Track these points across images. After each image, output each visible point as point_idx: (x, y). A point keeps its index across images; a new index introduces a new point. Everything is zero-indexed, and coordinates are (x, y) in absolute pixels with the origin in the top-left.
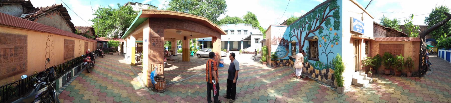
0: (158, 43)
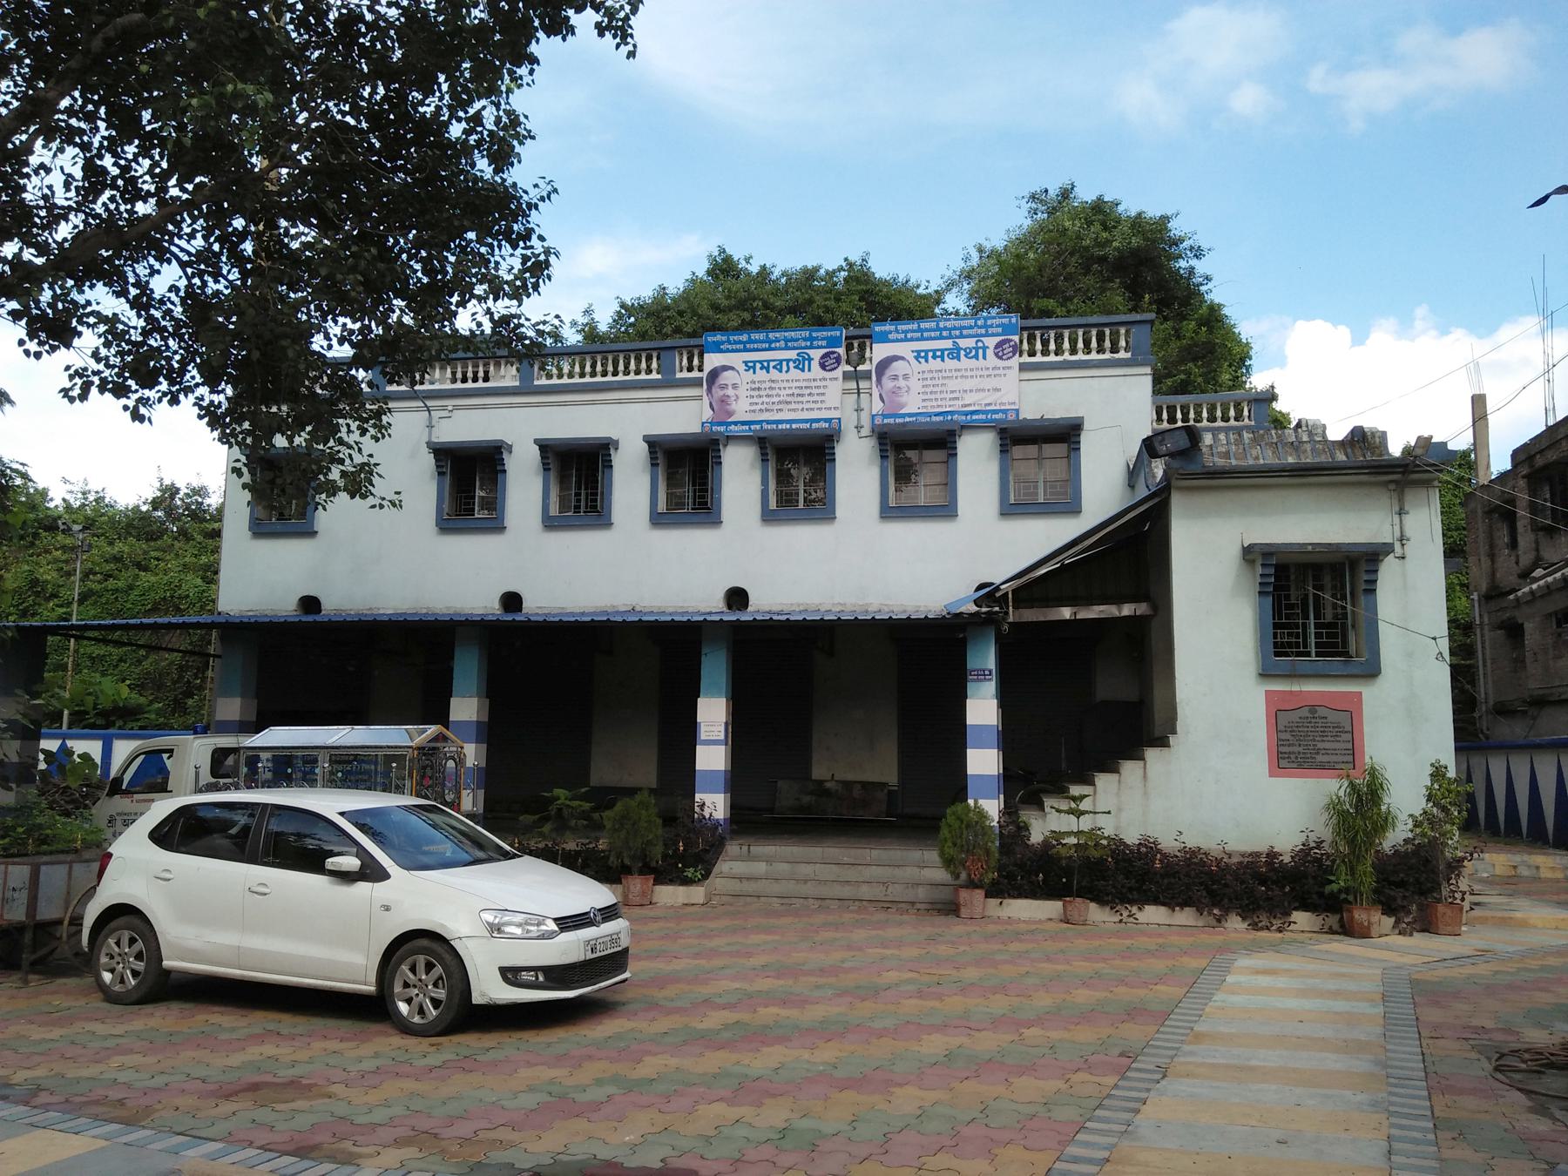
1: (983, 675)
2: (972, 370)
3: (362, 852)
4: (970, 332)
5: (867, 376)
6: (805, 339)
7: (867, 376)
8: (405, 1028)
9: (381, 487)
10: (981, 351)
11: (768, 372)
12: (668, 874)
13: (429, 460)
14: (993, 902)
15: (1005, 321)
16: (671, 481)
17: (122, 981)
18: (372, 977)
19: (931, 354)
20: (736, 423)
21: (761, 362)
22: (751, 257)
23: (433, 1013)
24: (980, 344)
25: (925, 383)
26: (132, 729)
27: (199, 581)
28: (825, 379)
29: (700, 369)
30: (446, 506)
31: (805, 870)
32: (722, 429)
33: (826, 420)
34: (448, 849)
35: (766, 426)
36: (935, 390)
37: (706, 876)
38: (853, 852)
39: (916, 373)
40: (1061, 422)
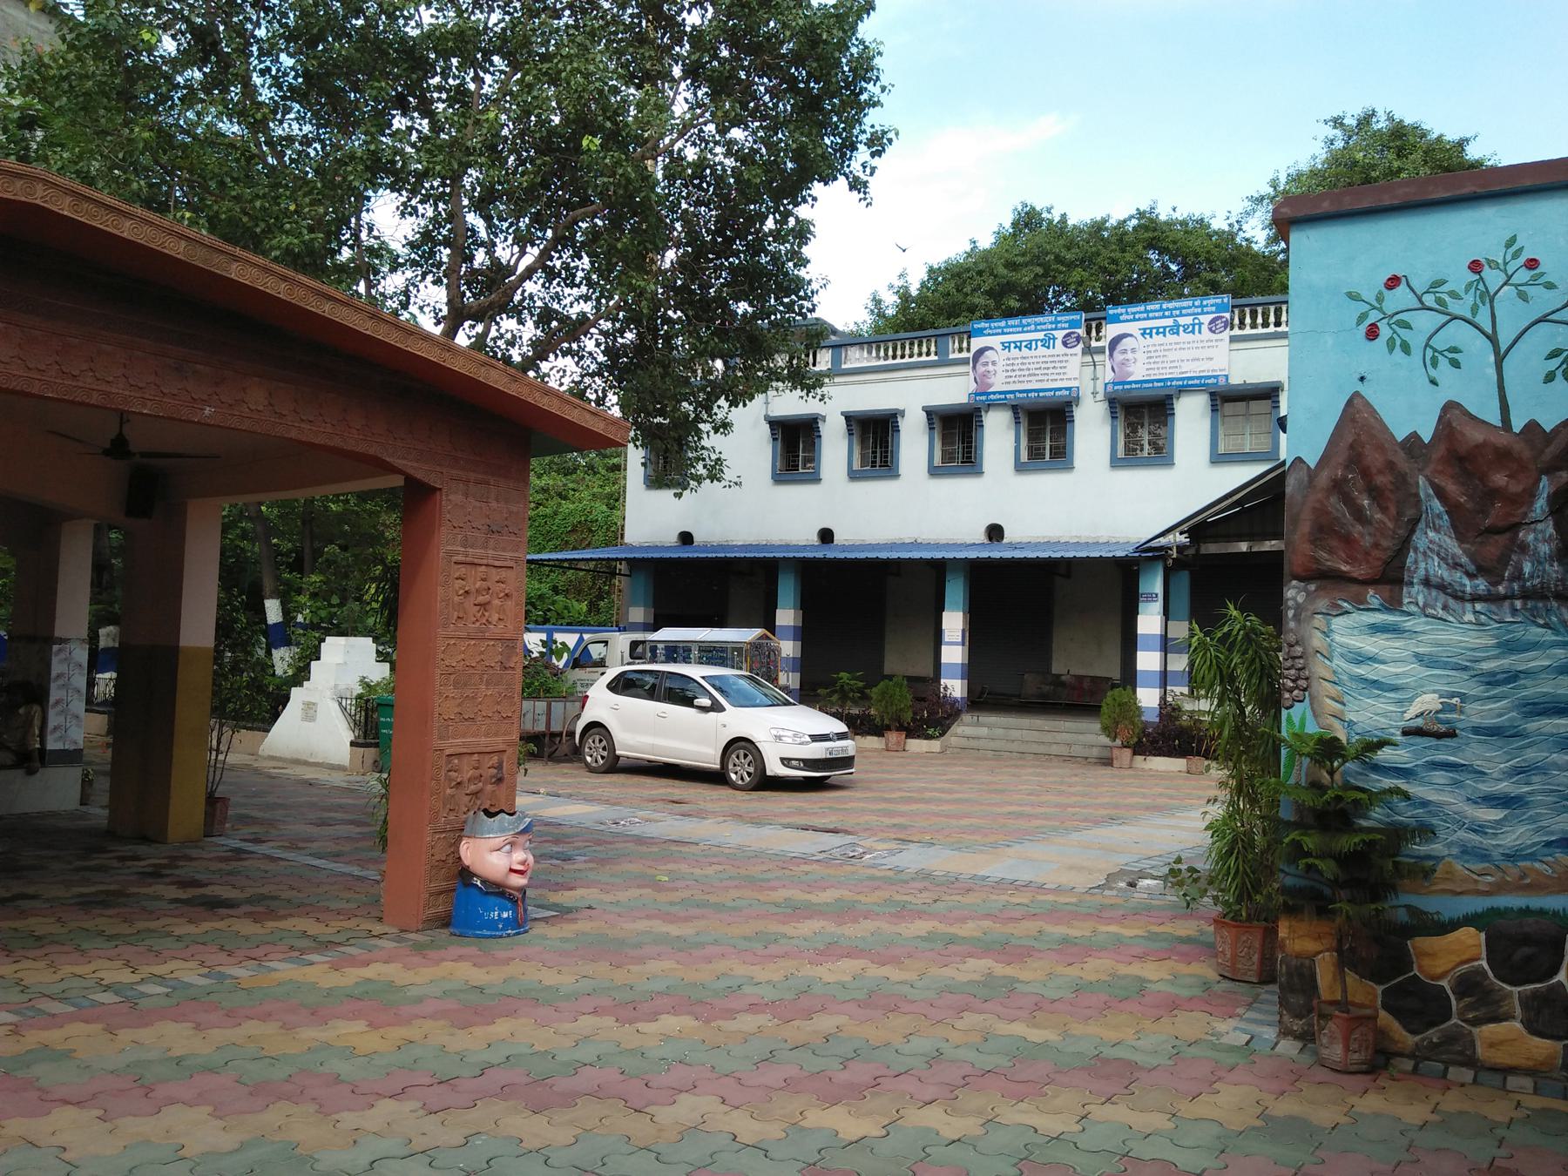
0: (489, 603)
1: (1152, 597)
2: (1189, 343)
3: (711, 697)
4: (1189, 311)
5: (1101, 351)
6: (1051, 323)
7: (1101, 351)
8: (735, 787)
9: (729, 475)
10: (1197, 327)
11: (1020, 350)
12: (914, 731)
13: (765, 429)
14: (1139, 758)
15: (1219, 301)
16: (945, 441)
17: (596, 761)
18: (718, 761)
19: (1154, 331)
20: (994, 393)
21: (1014, 342)
22: (1052, 207)
23: (748, 779)
24: (1196, 321)
25: (1149, 355)
26: (562, 625)
27: (604, 508)
28: (1066, 355)
29: (968, 350)
30: (778, 464)
31: (1015, 734)
32: (984, 398)
33: (1066, 389)
34: (761, 698)
35: (1018, 395)
36: (1157, 360)
37: (942, 735)
38: (1052, 723)
39: (1142, 346)
40: (1260, 386)
